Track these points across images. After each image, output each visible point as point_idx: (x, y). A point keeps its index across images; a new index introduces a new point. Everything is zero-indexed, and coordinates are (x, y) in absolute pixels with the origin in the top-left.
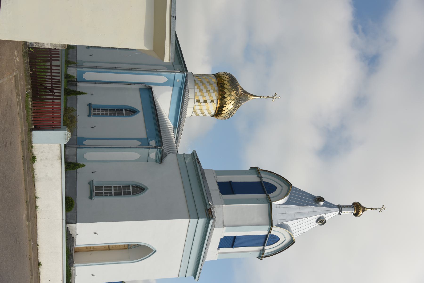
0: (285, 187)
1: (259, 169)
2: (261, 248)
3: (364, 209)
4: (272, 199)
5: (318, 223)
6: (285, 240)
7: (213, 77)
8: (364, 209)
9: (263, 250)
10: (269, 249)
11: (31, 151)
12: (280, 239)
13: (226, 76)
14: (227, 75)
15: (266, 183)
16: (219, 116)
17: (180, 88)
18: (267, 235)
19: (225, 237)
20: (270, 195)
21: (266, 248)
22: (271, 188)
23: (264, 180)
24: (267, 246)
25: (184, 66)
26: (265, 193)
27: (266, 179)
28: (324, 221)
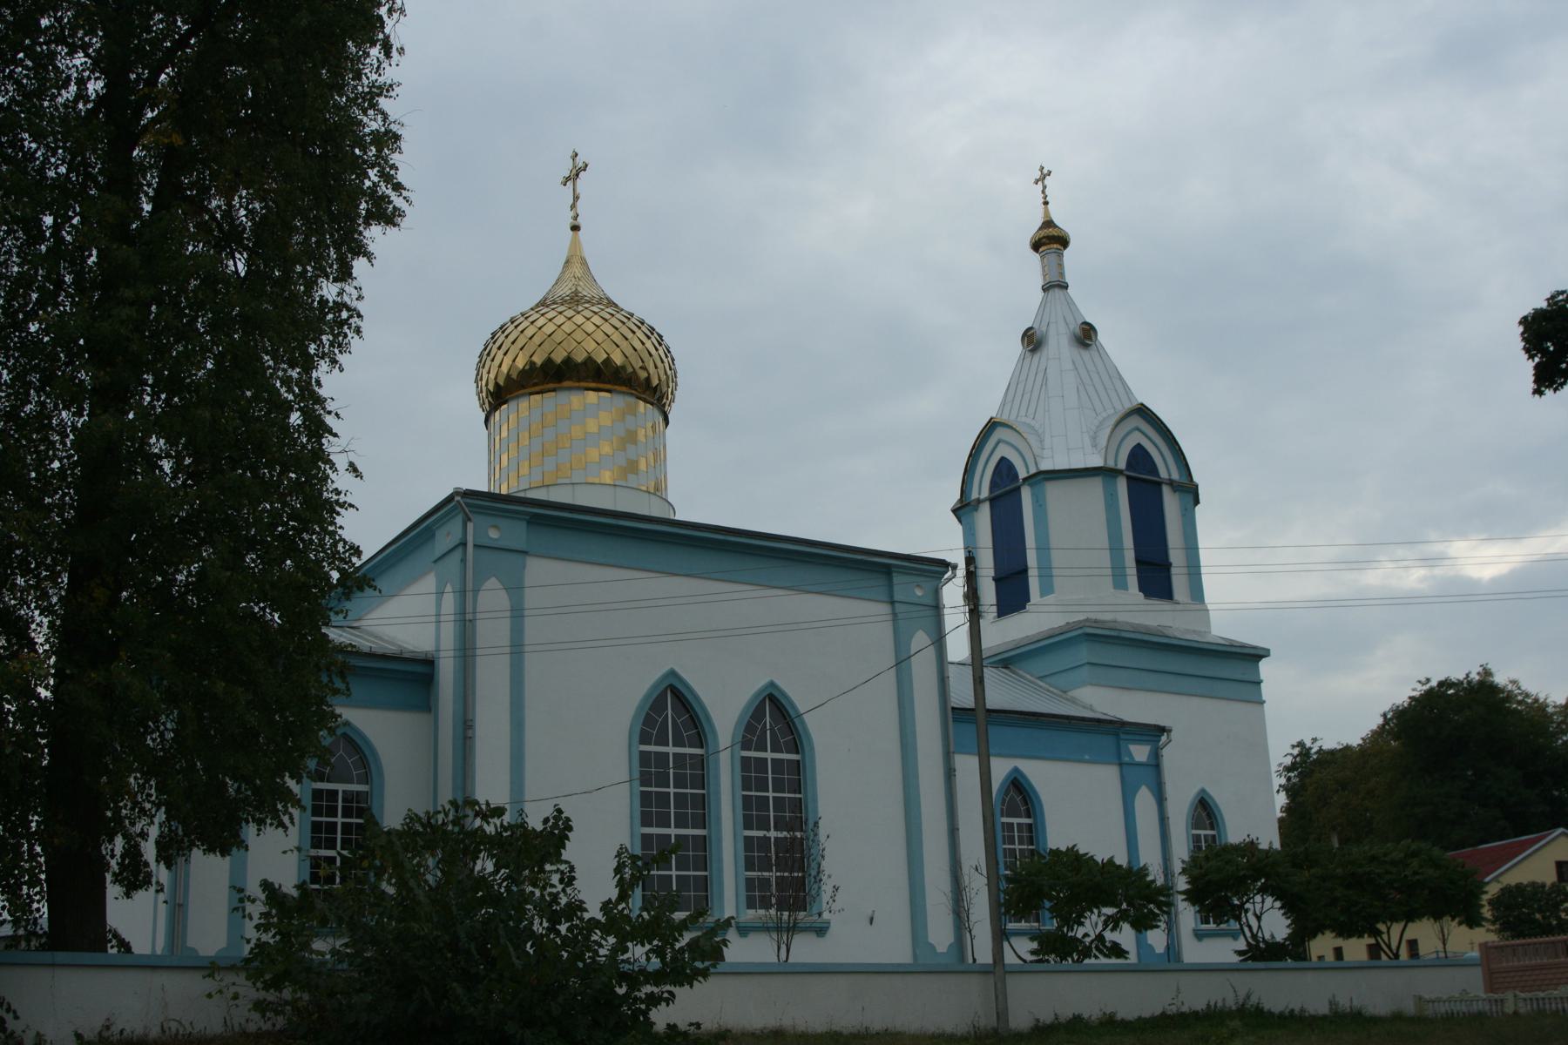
0: (1000, 433)
1: (959, 505)
2: (1166, 490)
3: (1048, 223)
4: (1033, 470)
5: (1090, 343)
6: (1137, 432)
7: (504, 416)
8: (1048, 223)
9: (1171, 483)
10: (1166, 469)
11: (1375, 1021)
12: (1139, 444)
13: (497, 362)
14: (492, 355)
15: (994, 485)
16: (657, 382)
17: (529, 523)
18: (1129, 478)
19: (1141, 590)
20: (1022, 474)
21: (1163, 474)
22: (1005, 470)
23: (985, 493)
24: (1158, 475)
25: (439, 514)
26: (1018, 489)
27: (982, 489)
28: (1084, 326)
